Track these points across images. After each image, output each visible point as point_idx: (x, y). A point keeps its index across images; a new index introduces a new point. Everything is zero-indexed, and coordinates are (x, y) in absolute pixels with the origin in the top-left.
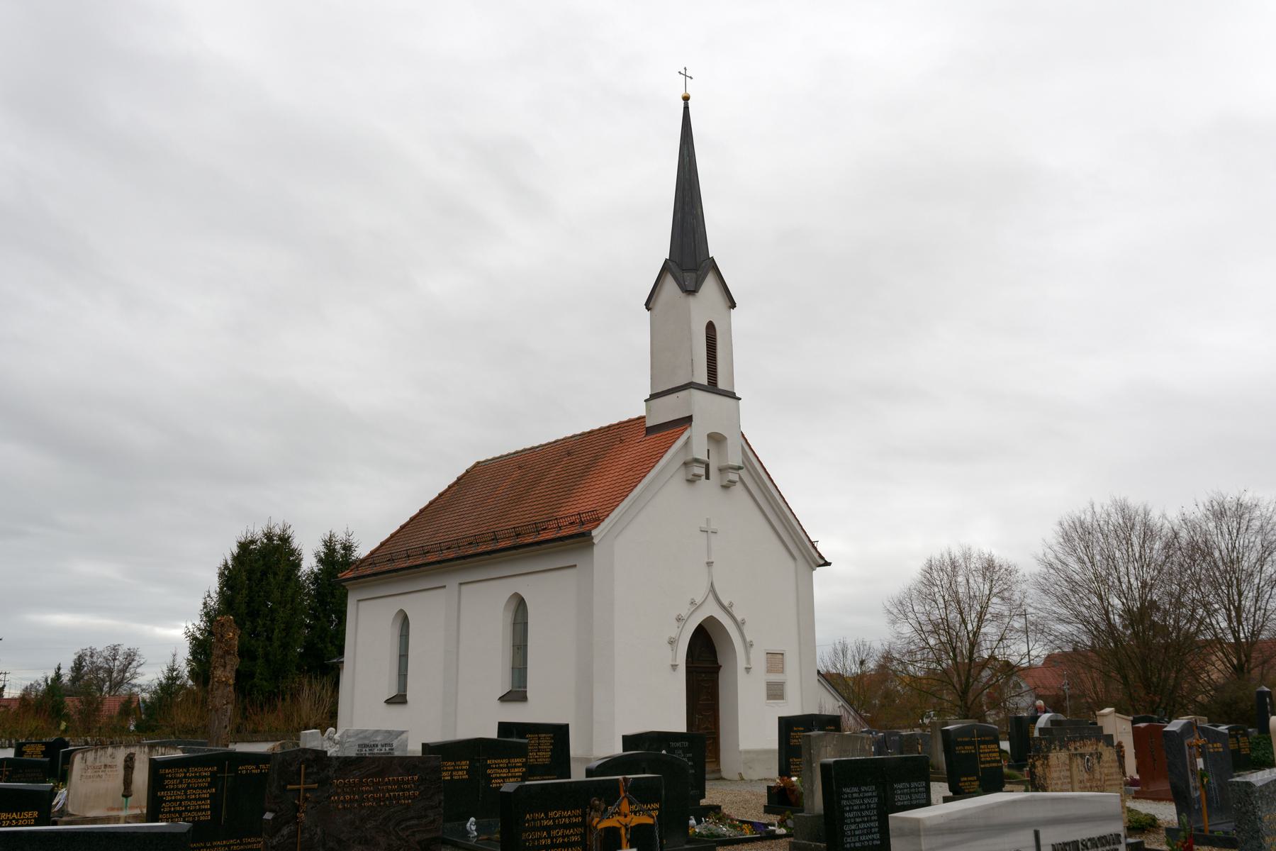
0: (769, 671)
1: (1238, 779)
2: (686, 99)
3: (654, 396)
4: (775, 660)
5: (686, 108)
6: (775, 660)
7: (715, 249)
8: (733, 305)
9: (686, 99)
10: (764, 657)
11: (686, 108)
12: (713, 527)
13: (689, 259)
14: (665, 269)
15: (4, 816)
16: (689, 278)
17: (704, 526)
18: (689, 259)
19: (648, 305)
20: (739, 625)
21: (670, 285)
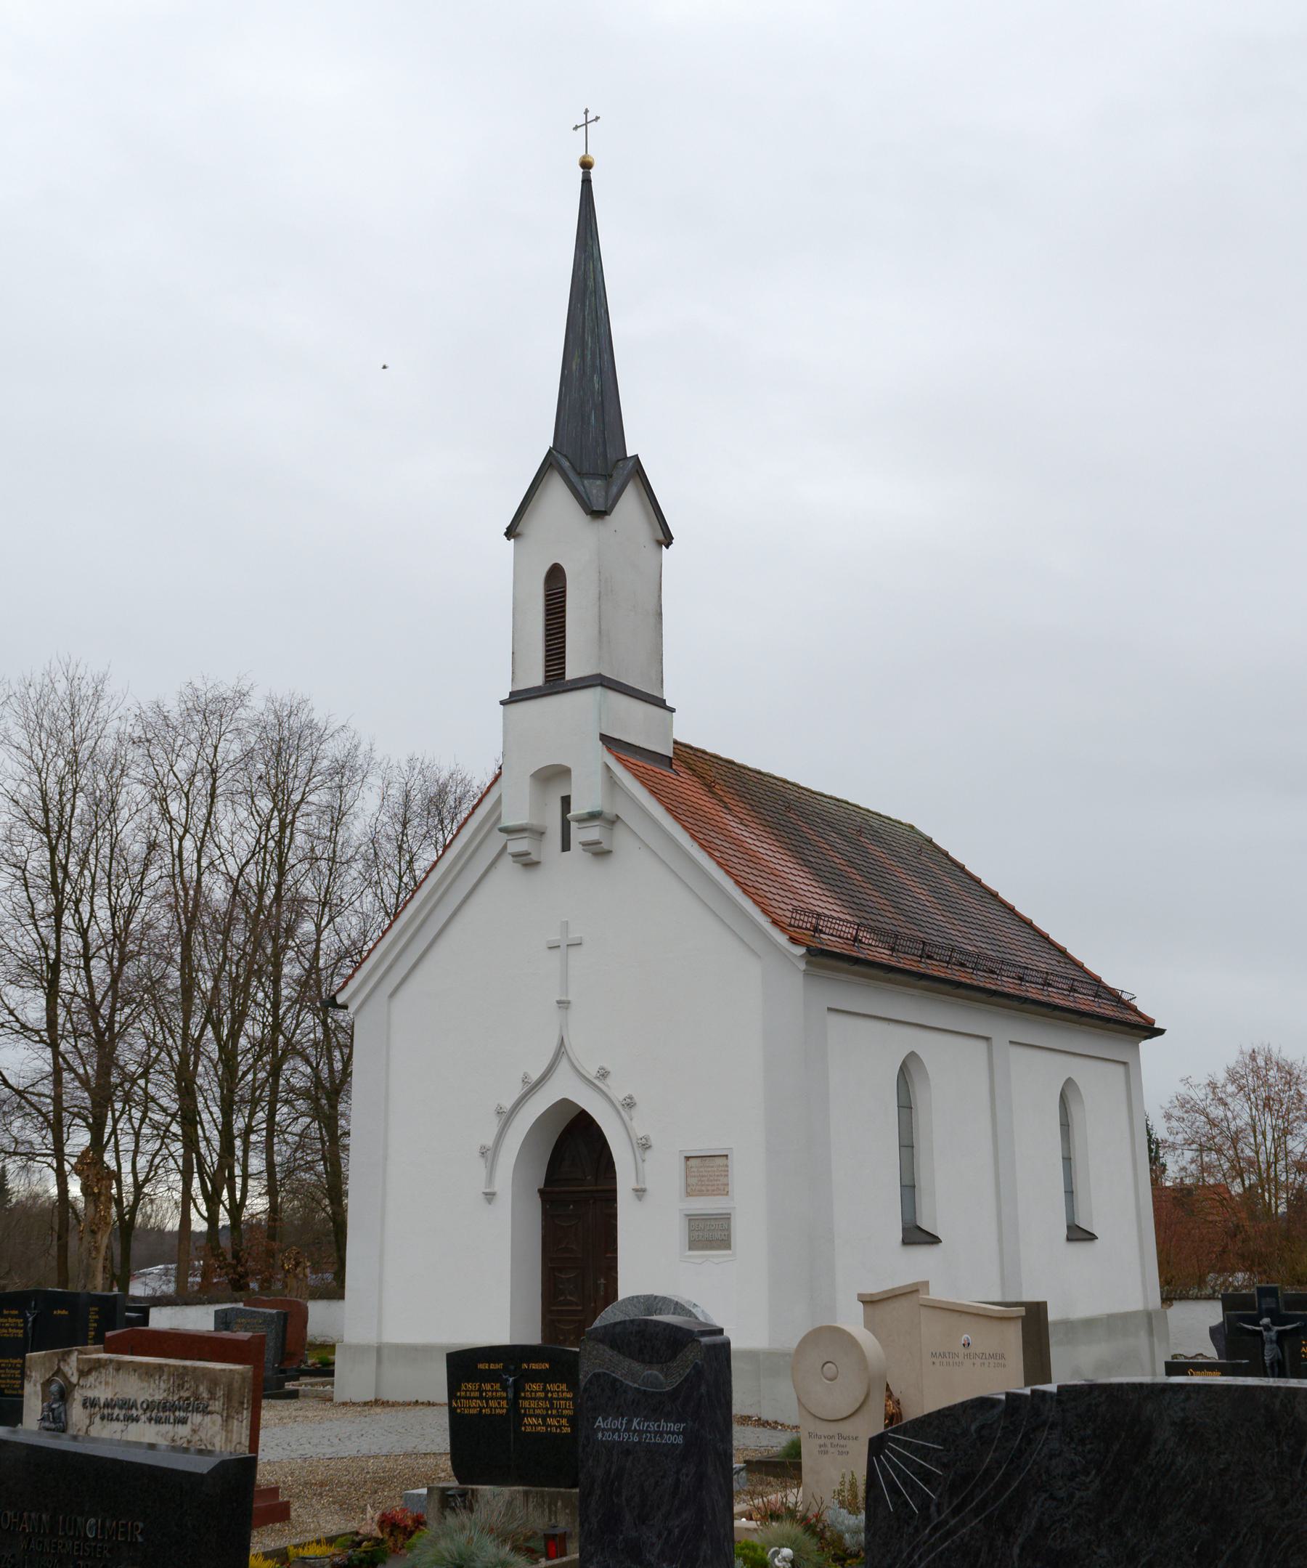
0: (690, 1191)
1: (415, 1491)
2: (586, 165)
3: (516, 697)
4: (706, 1170)
5: (586, 182)
6: (706, 1170)
7: (638, 440)
8: (666, 539)
9: (586, 165)
10: (678, 1166)
11: (586, 182)
12: (574, 935)
13: (590, 453)
14: (549, 464)
15: (5, 1312)
16: (595, 488)
17: (555, 937)
18: (590, 453)
19: (511, 533)
20: (507, 1117)
21: (558, 495)
